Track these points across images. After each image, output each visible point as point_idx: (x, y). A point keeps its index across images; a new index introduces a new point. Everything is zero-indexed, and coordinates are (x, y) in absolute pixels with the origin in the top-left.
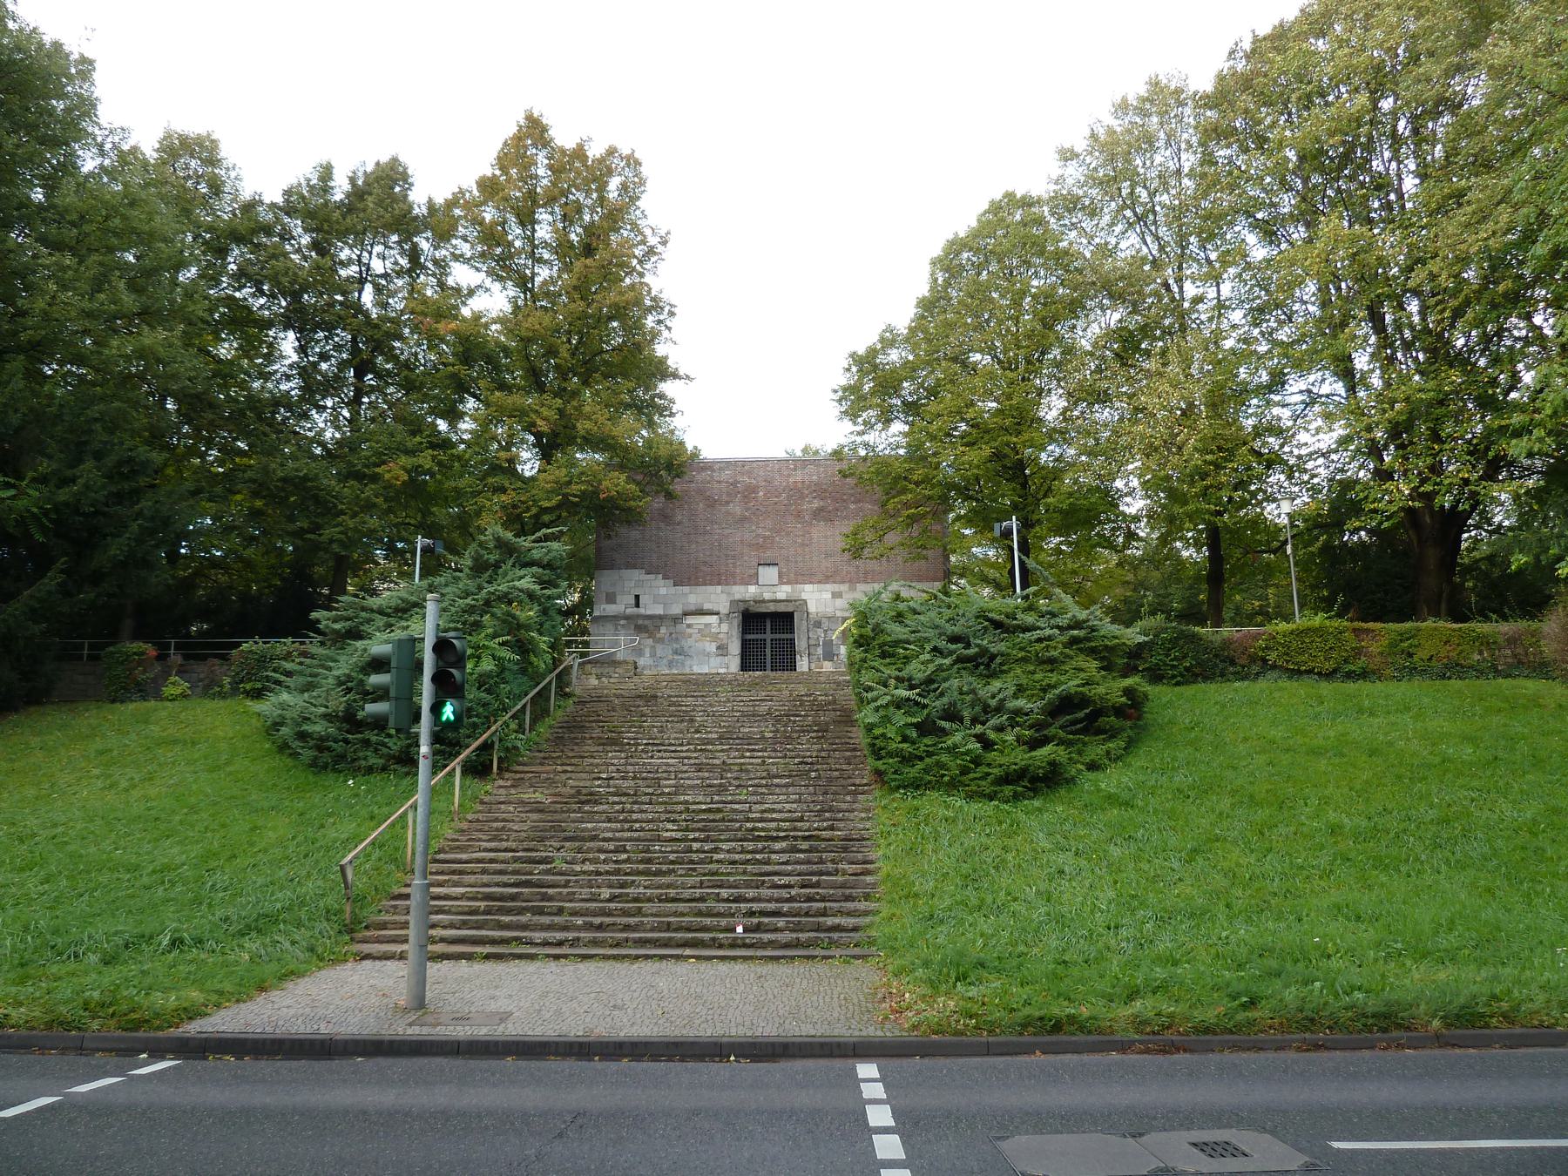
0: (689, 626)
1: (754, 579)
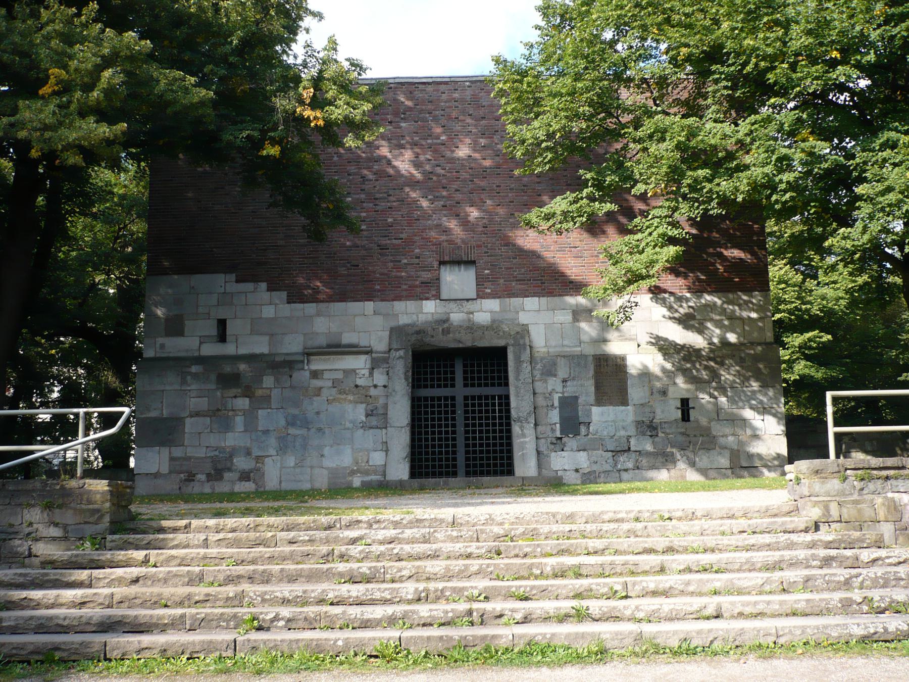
0: (315, 374)
1: (431, 289)
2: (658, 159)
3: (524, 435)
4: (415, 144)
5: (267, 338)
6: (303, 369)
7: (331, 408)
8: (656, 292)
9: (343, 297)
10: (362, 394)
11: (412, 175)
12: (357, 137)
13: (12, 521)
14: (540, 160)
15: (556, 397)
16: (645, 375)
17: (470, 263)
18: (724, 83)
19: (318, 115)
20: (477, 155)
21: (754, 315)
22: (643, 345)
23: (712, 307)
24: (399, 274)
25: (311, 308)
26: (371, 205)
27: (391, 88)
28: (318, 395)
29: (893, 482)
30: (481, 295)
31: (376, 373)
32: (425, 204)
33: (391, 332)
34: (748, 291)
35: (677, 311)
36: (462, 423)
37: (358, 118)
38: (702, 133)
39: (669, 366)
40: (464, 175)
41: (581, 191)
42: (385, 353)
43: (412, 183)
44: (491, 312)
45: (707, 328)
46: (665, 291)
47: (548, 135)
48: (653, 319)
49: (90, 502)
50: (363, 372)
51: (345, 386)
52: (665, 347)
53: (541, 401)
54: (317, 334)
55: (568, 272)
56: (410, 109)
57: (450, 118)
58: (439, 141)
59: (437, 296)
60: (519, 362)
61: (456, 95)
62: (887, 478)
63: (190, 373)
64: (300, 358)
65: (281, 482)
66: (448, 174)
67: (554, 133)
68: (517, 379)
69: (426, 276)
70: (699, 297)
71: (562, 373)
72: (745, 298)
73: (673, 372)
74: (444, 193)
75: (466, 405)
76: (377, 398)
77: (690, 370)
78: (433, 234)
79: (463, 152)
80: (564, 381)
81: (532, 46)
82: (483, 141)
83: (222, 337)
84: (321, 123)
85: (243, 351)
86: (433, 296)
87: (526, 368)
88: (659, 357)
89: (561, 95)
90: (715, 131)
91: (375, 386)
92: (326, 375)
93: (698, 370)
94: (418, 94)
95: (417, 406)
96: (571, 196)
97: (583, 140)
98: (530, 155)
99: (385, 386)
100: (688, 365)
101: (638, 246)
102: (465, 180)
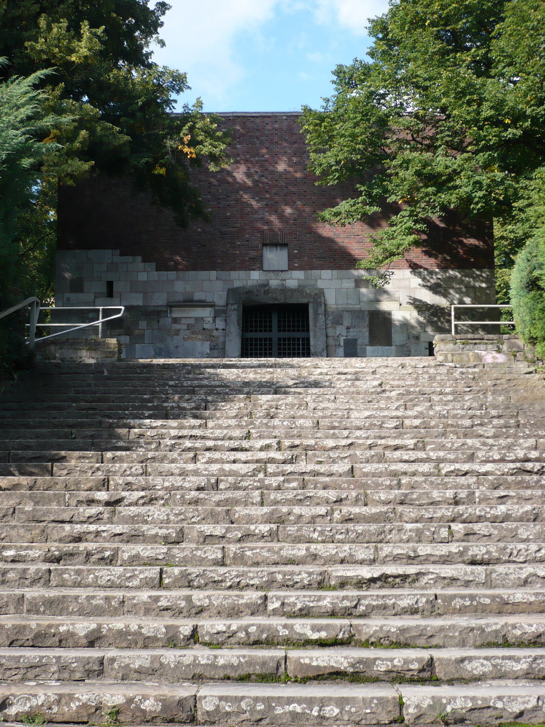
0: (176, 320)
1: (256, 263)
2: (403, 180)
4: (246, 161)
5: (142, 295)
6: (167, 317)
8: (414, 267)
9: (195, 268)
10: (207, 334)
11: (245, 182)
12: (216, 165)
13: (72, 356)
14: (331, 177)
15: (342, 339)
16: (405, 325)
17: (284, 245)
18: (447, 133)
19: (193, 151)
20: (291, 169)
21: (484, 285)
22: (405, 305)
23: (452, 279)
24: (234, 252)
25: (172, 275)
26: (215, 203)
28: (177, 335)
29: (478, 346)
30: (291, 268)
31: (218, 320)
32: (254, 203)
33: (228, 292)
34: (480, 268)
35: (429, 281)
36: (278, 327)
37: (217, 153)
38: (434, 164)
39: (421, 319)
40: (282, 183)
41: (358, 198)
42: (224, 306)
43: (244, 188)
45: (450, 294)
46: (421, 267)
47: (336, 162)
48: (412, 287)
49: (108, 348)
50: (209, 319)
51: (196, 328)
52: (420, 306)
53: (331, 342)
55: (353, 253)
56: (243, 135)
57: (271, 142)
58: (263, 159)
59: (261, 268)
60: (316, 314)
61: (276, 126)
62: (475, 344)
64: (165, 309)
66: (270, 183)
67: (340, 161)
68: (315, 325)
69: (253, 254)
70: (445, 272)
71: (347, 322)
72: (478, 273)
73: (424, 324)
74: (267, 196)
75: (279, 345)
76: (218, 337)
77: (436, 322)
78: (259, 225)
79: (281, 167)
80: (348, 328)
81: (328, 100)
82: (295, 159)
84: (194, 156)
86: (258, 268)
87: (322, 318)
88: (415, 313)
89: (345, 137)
90: (442, 162)
91: (217, 329)
92: (183, 321)
93: (442, 323)
94: (249, 125)
96: (352, 202)
97: (360, 164)
98: (325, 173)
99: (223, 330)
100: (436, 319)
101: (393, 235)
102: (281, 187)
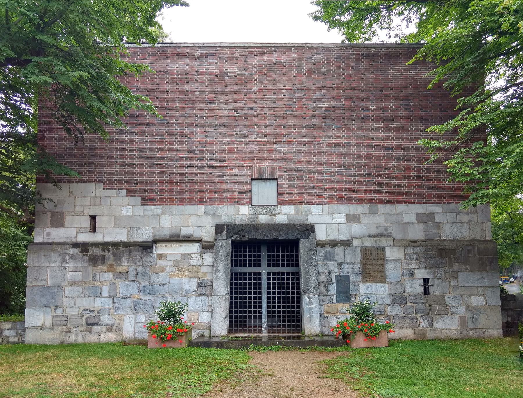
0: (161, 256)
3: (310, 303)
5: (126, 230)
7: (172, 281)
10: (194, 271)
15: (334, 276)
27: (218, 51)
30: (281, 202)
44: (288, 214)
54: (163, 227)
59: (250, 203)
61: (265, 57)
63: (68, 254)
65: (135, 333)
69: (244, 188)
83: (94, 230)
85: (108, 239)
95: (235, 280)
